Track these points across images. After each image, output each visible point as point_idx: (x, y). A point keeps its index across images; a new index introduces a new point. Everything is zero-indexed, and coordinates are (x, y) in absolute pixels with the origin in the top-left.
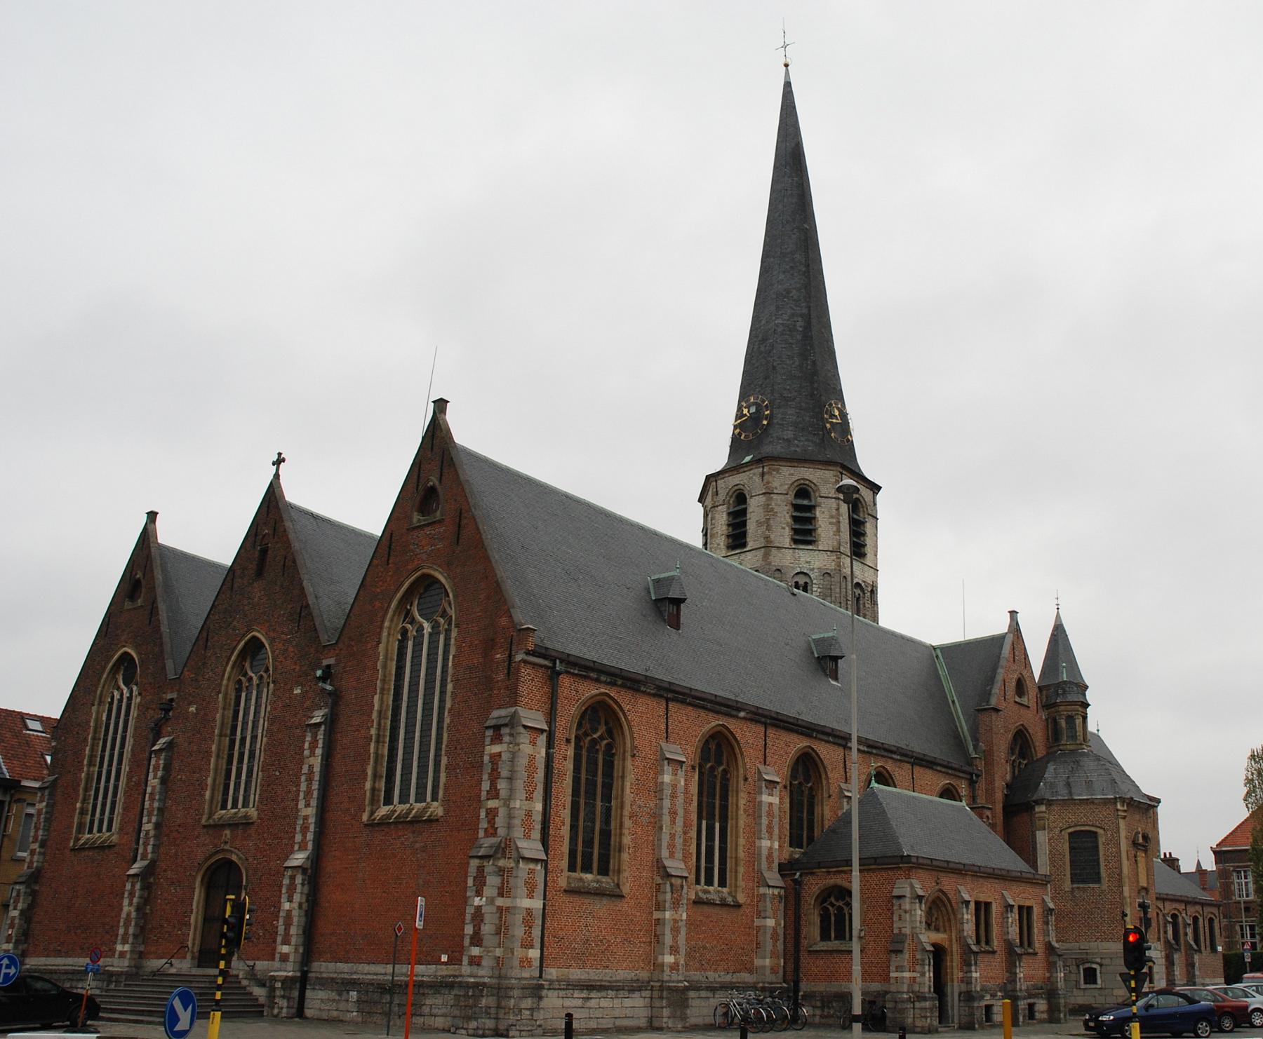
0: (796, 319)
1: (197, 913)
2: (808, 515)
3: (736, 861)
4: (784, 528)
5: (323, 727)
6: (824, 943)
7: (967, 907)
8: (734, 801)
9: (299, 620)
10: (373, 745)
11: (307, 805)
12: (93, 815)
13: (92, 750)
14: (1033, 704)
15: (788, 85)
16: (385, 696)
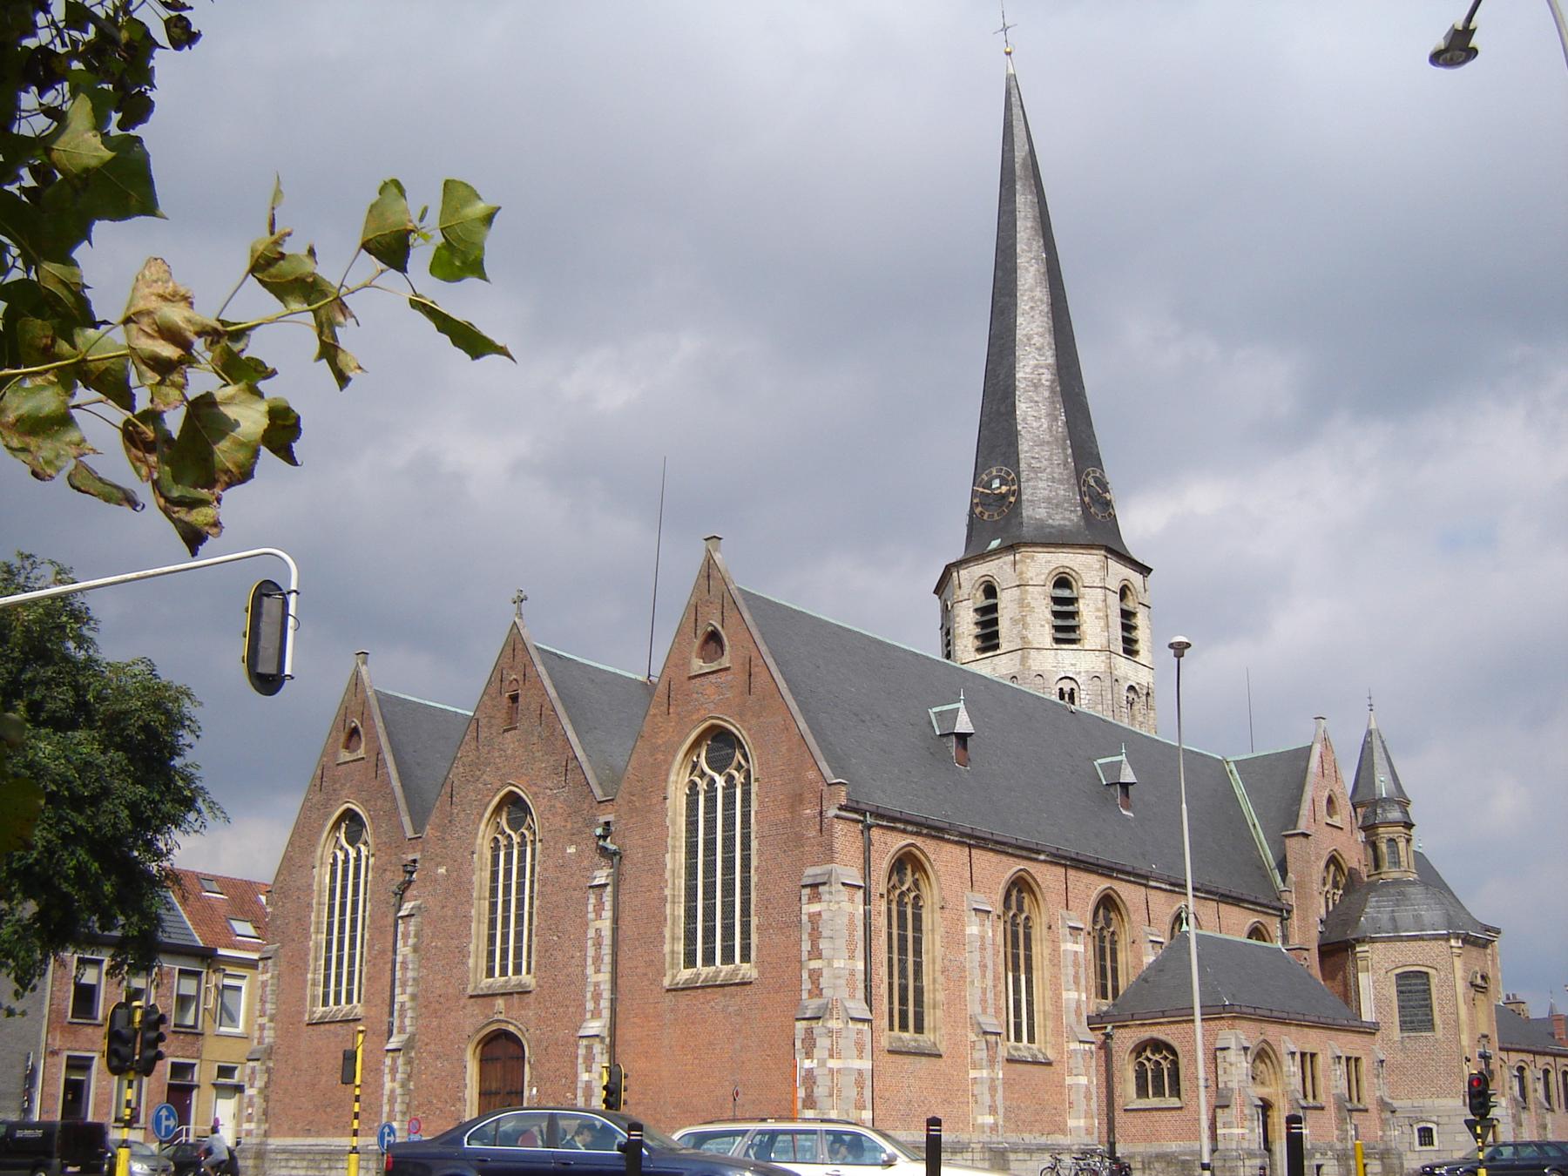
0: (1041, 371)
2: (1070, 608)
3: (1044, 1015)
4: (1042, 626)
5: (609, 889)
6: (1141, 1101)
7: (1293, 1058)
8: (1039, 951)
9: (566, 775)
10: (668, 906)
11: (598, 971)
13: (318, 916)
14: (1347, 828)
16: (677, 855)
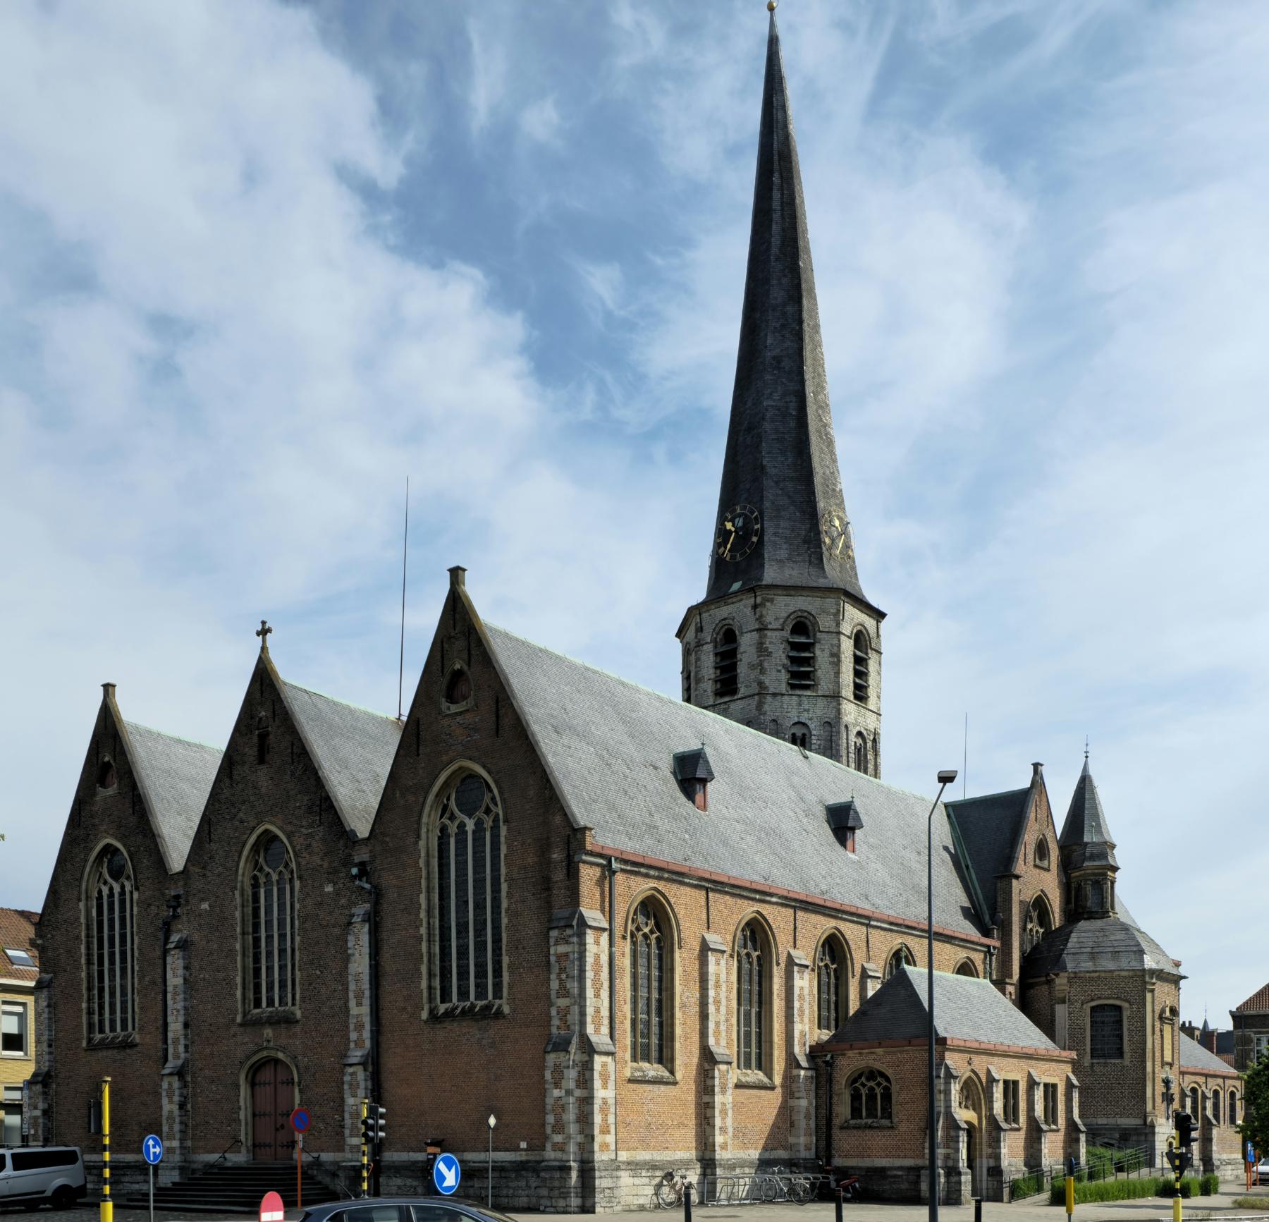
1: (246, 1108)
4: (779, 671)
12: (101, 1014)
15: (773, 42)
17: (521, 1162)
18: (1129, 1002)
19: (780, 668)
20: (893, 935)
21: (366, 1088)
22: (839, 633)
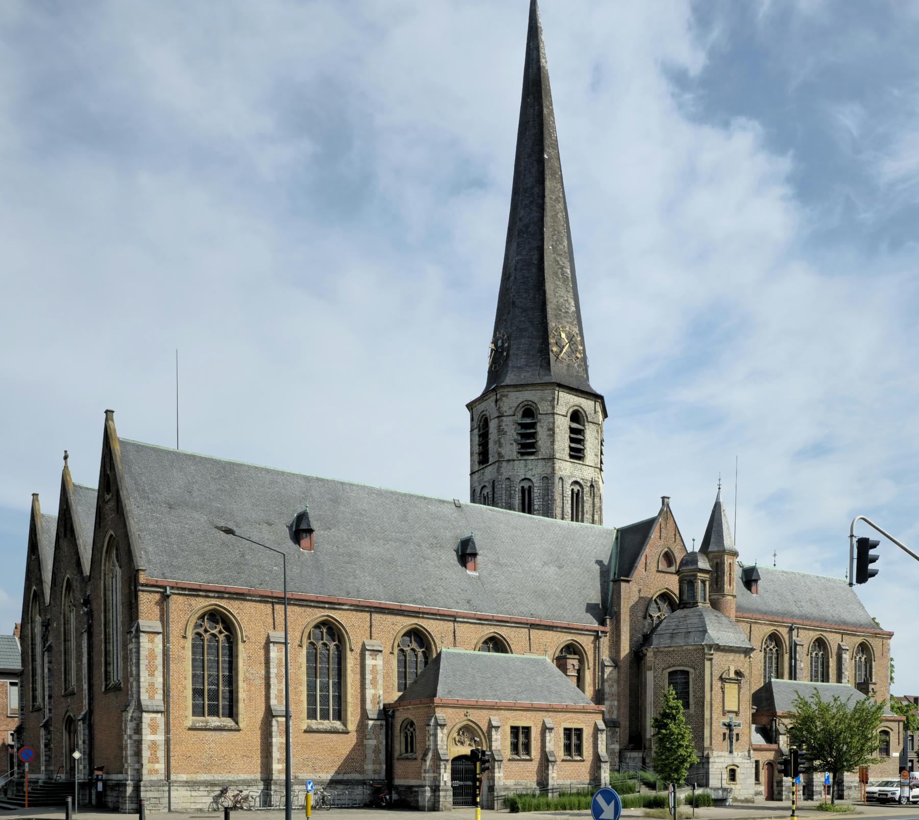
4: (512, 444)
17: (600, 780)
18: (694, 668)
19: (512, 442)
20: (485, 627)
21: (84, 735)
22: (553, 414)
